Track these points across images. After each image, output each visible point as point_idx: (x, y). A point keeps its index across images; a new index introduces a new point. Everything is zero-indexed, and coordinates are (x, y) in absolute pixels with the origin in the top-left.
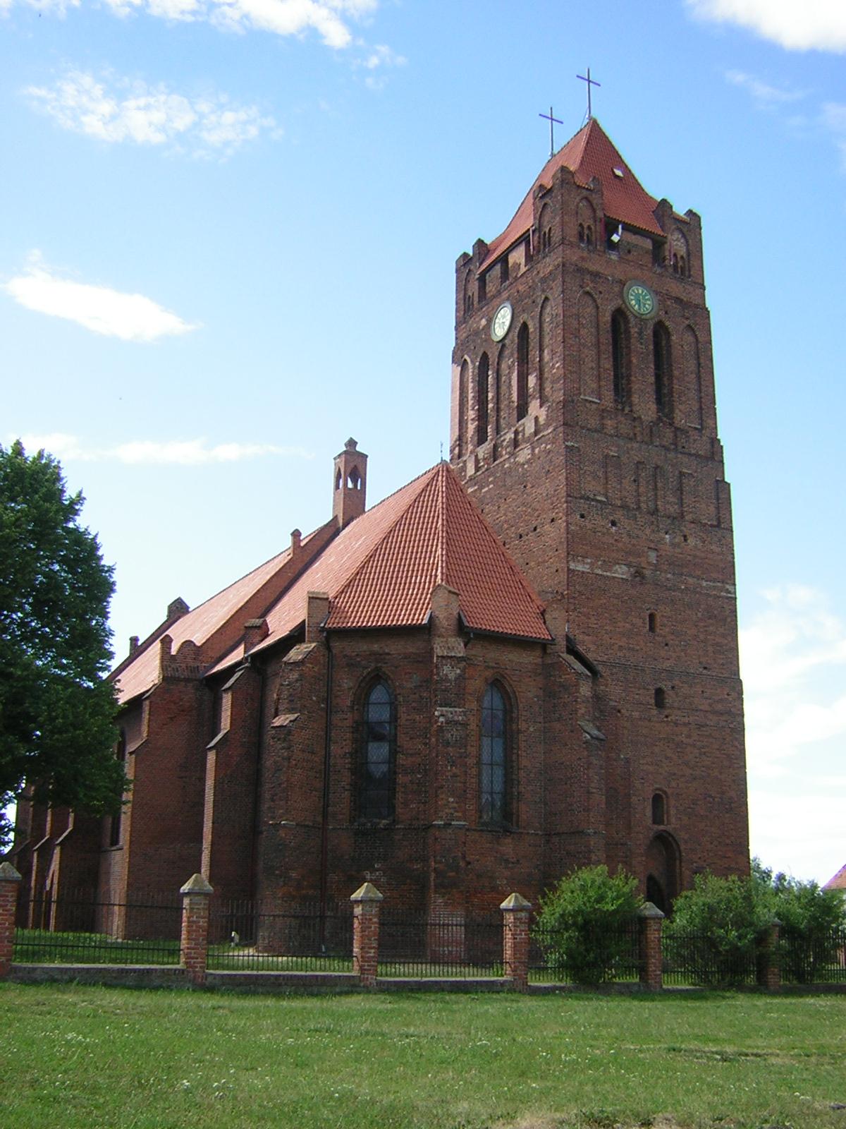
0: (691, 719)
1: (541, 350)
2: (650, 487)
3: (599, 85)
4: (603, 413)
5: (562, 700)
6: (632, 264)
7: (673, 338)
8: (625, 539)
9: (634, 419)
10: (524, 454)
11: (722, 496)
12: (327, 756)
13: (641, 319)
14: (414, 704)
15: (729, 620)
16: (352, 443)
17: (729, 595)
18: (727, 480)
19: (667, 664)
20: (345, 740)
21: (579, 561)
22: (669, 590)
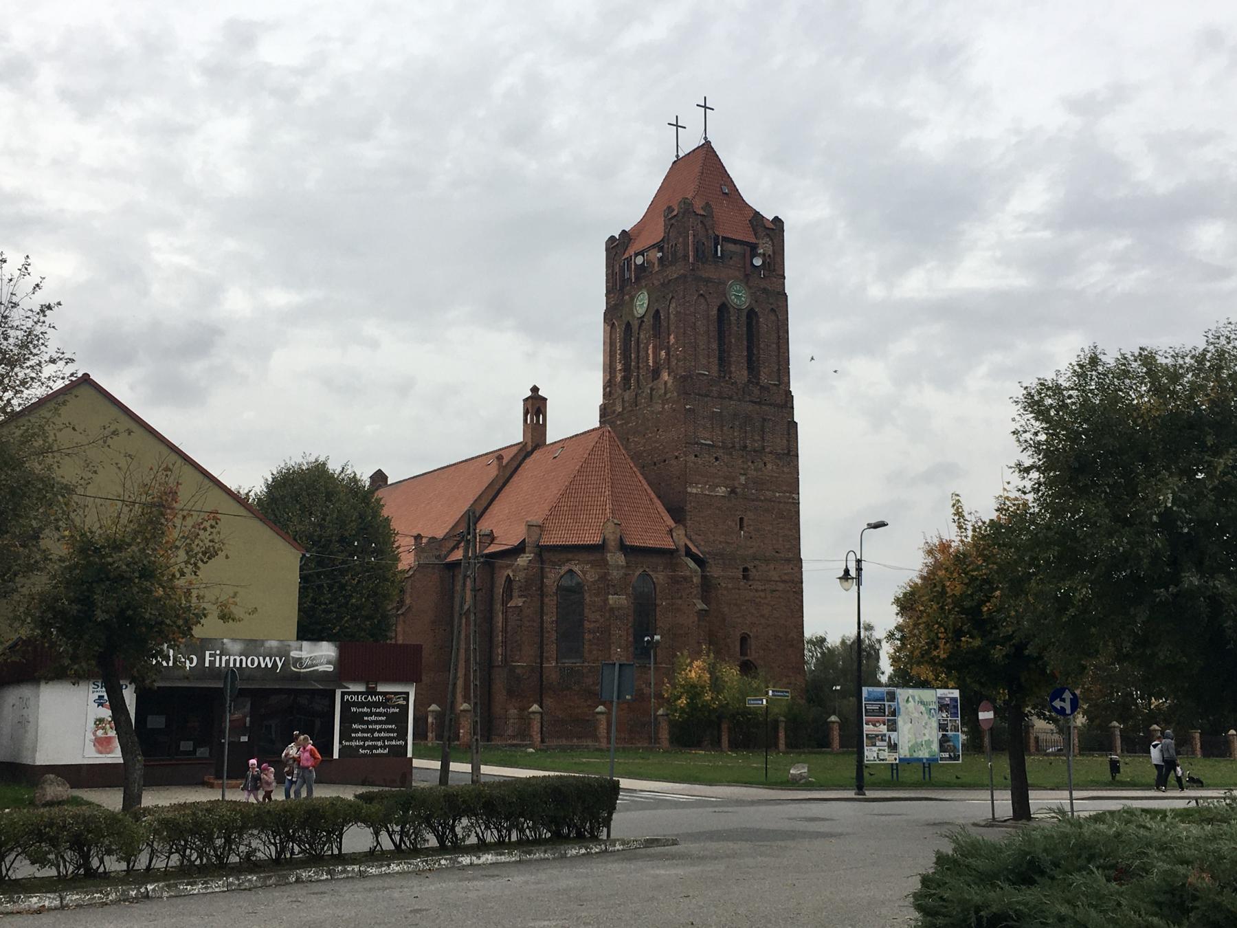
12: (542, 622)
16: (535, 389)
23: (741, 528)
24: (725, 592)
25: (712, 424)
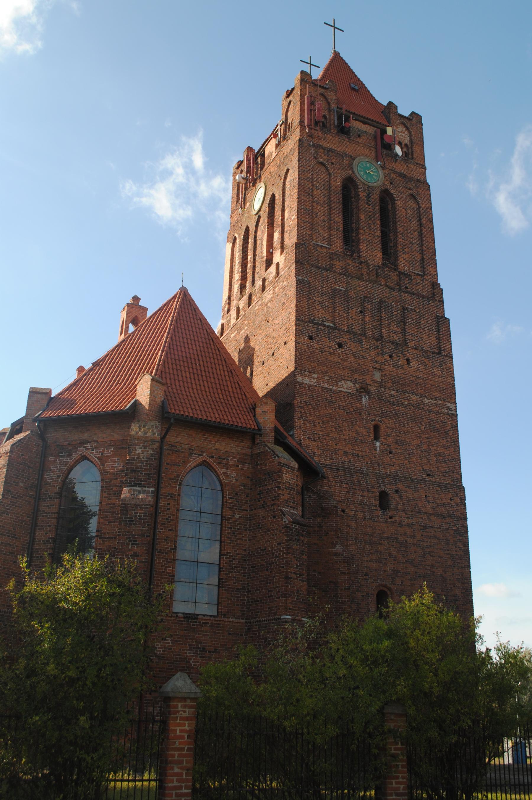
0: (415, 521)
1: (283, 210)
2: (376, 318)
3: (343, 31)
4: (332, 256)
5: (267, 487)
6: (362, 145)
7: (398, 203)
8: (351, 359)
9: (361, 263)
10: (268, 295)
11: (442, 328)
13: (370, 189)
14: (114, 489)
15: (450, 433)
16: (136, 299)
17: (450, 412)
18: (446, 316)
19: (390, 470)
20: (50, 526)
21: (305, 376)
22: (394, 405)
23: (376, 438)
24: (353, 524)
25: (333, 303)
